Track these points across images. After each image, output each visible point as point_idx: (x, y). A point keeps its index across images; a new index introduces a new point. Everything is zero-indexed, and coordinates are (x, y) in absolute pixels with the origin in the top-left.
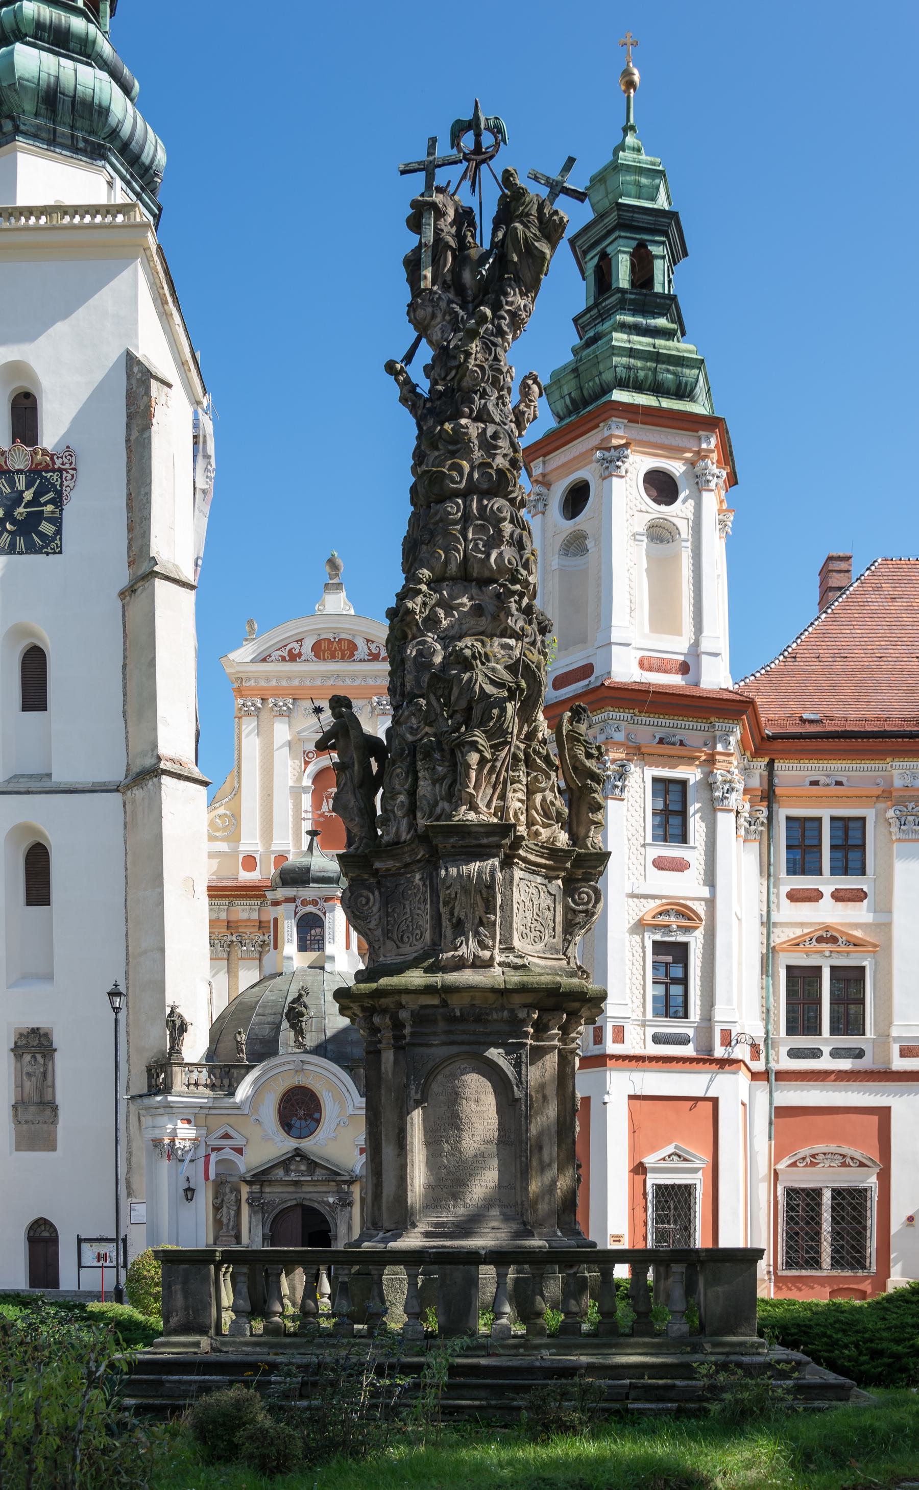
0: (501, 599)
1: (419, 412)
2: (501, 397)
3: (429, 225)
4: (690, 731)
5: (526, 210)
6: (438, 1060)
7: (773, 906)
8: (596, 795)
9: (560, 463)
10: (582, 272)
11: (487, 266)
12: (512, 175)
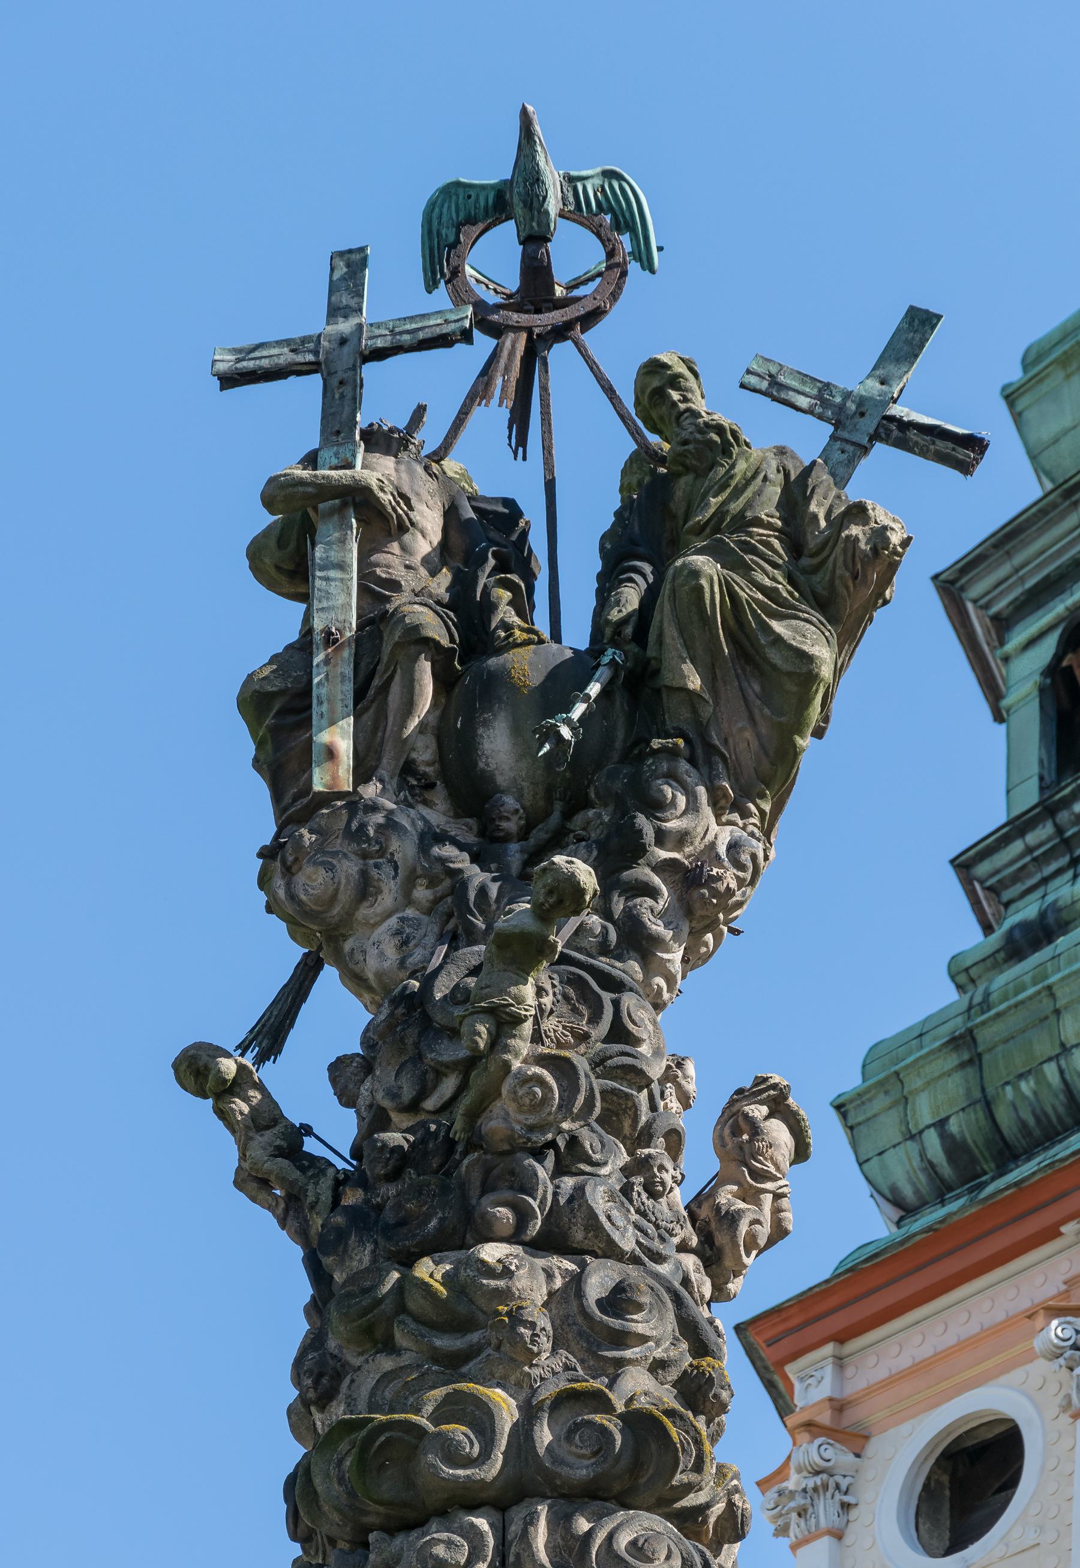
1: (317, 1223)
2: (640, 1166)
3: (342, 566)
5: (735, 507)
9: (905, 1361)
10: (993, 691)
11: (579, 710)
12: (675, 381)
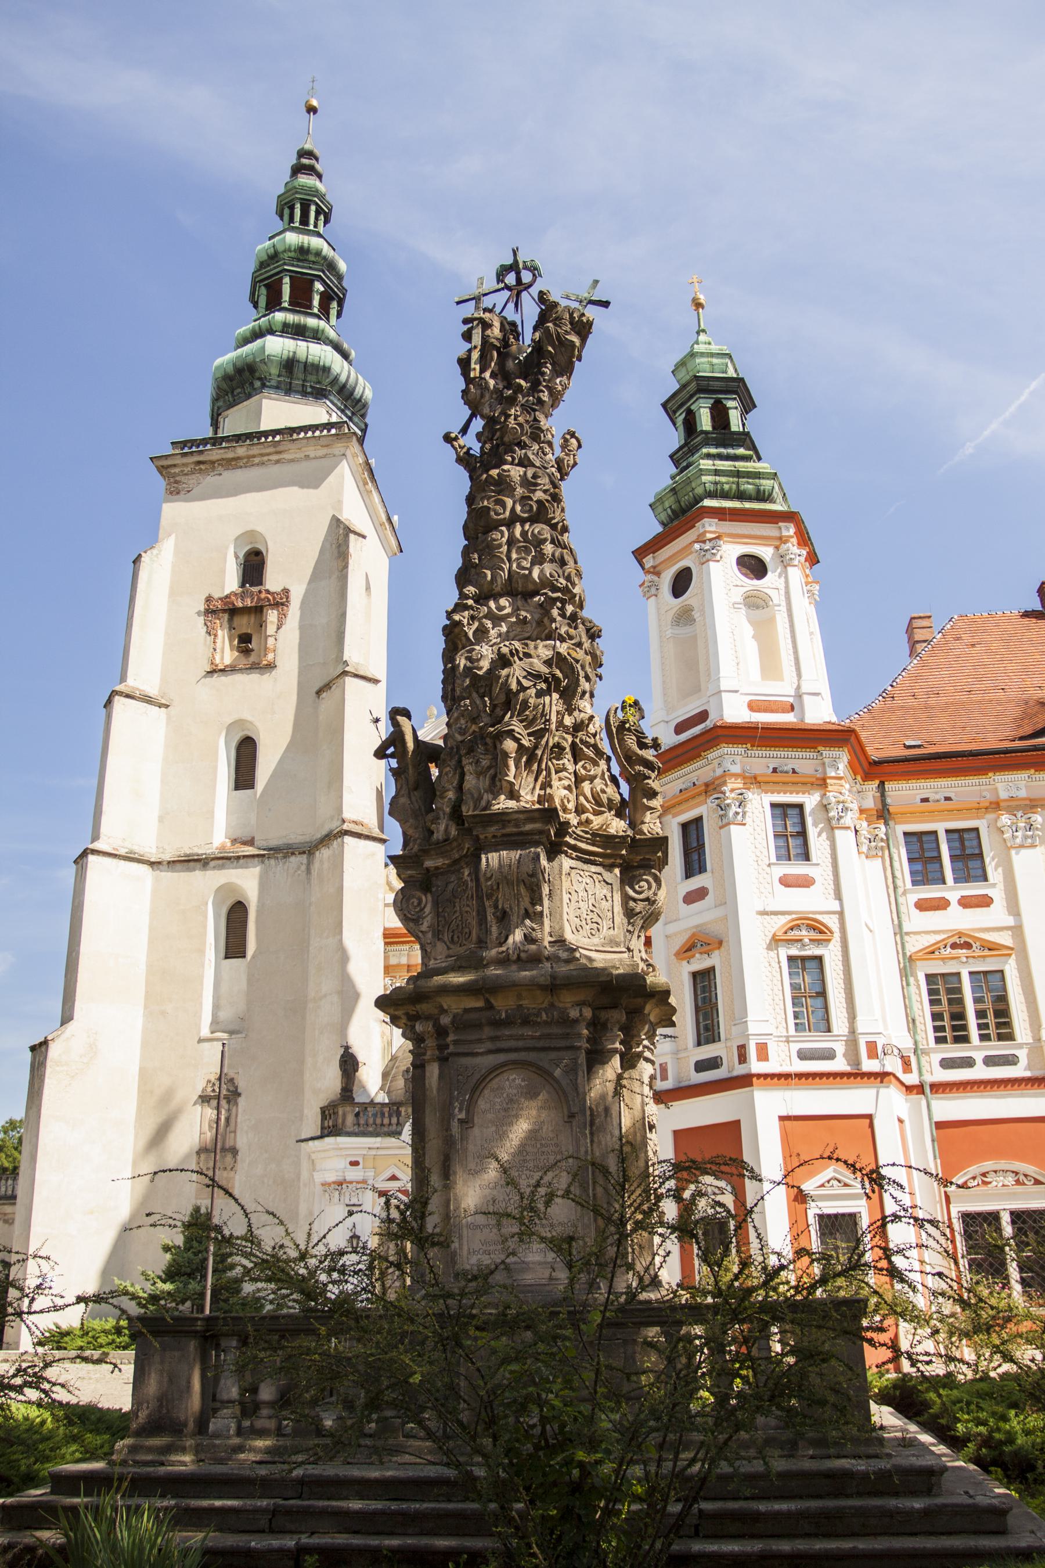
0: (545, 609)
4: (802, 761)
6: (484, 1071)
7: (904, 917)
8: (650, 781)
10: (674, 424)
